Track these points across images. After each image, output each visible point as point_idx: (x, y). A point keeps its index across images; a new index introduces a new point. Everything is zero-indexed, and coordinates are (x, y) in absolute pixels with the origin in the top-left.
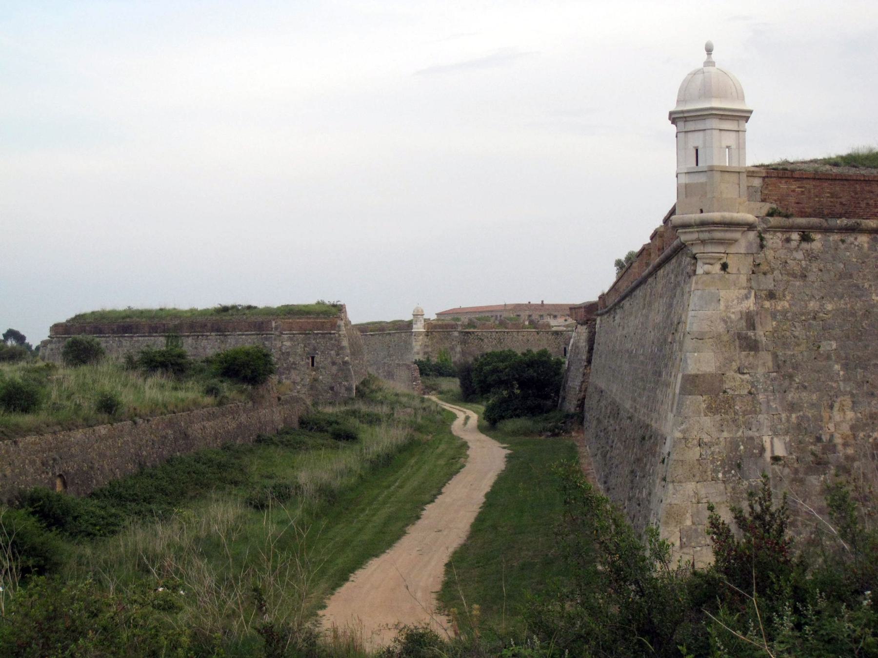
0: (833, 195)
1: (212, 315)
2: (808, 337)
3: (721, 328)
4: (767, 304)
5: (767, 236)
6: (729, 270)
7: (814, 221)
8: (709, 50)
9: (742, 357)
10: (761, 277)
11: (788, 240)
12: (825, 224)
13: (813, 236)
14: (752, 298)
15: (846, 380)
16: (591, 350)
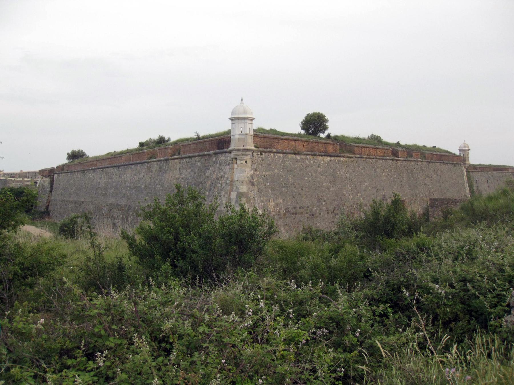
3: (247, 179)
7: (264, 149)
8: (242, 100)
9: (251, 187)
15: (272, 194)
16: (52, 187)
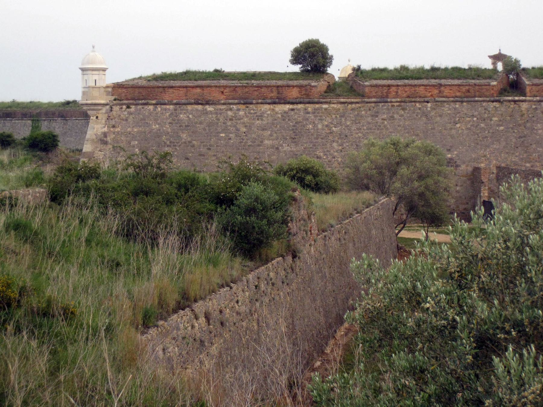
0: (139, 93)
1: (59, 106)
2: (126, 140)
3: (94, 137)
4: (112, 129)
5: (114, 107)
6: (99, 118)
7: (131, 101)
8: (93, 47)
10: (110, 121)
11: (121, 108)
12: (135, 103)
13: (131, 106)
14: (107, 127)
